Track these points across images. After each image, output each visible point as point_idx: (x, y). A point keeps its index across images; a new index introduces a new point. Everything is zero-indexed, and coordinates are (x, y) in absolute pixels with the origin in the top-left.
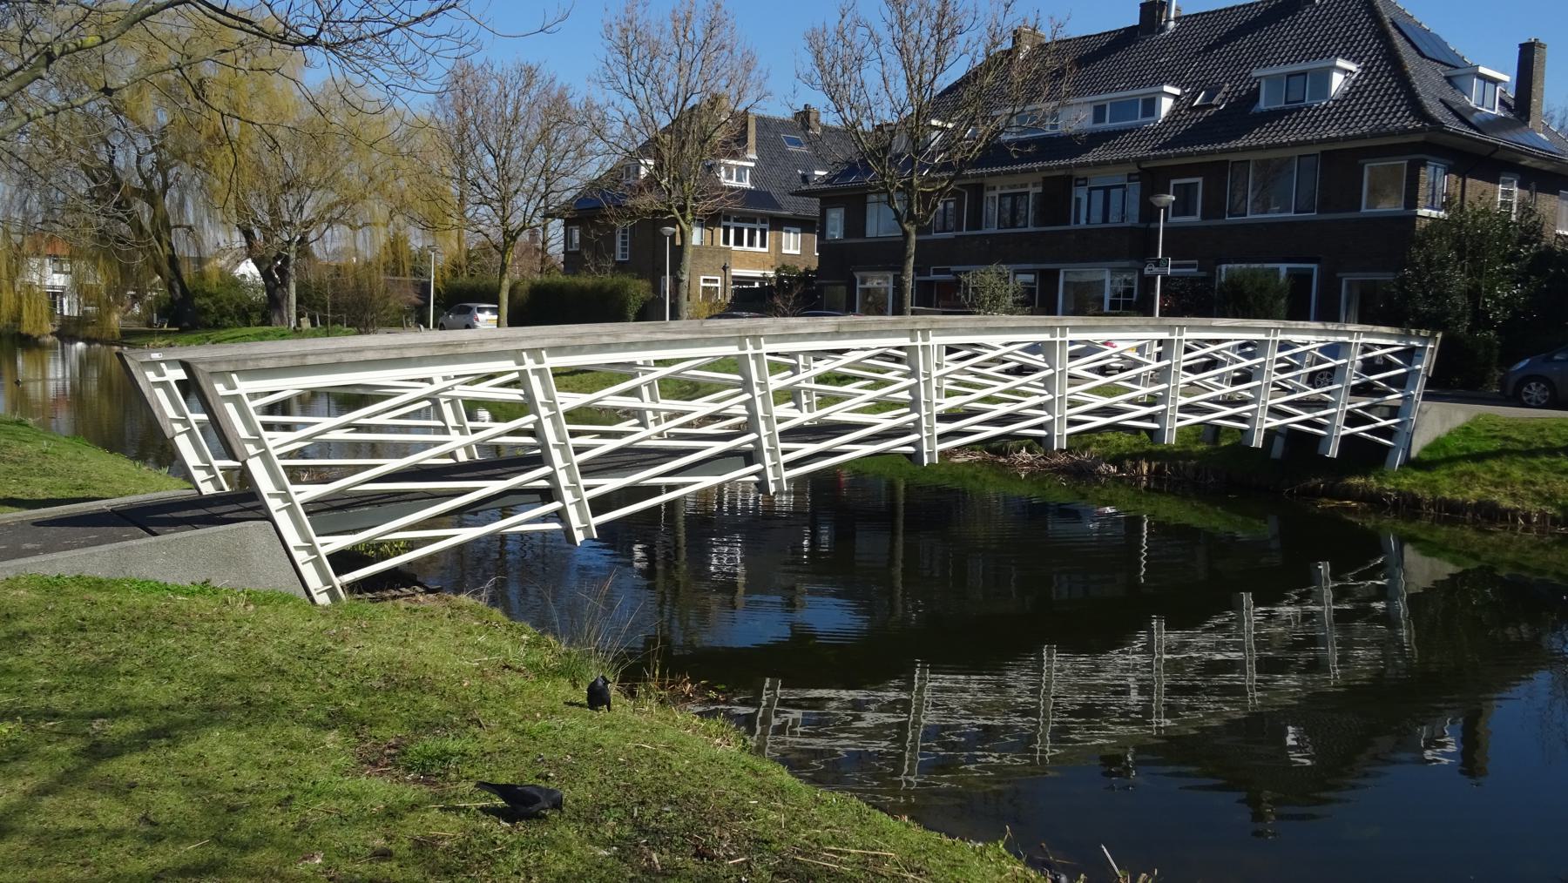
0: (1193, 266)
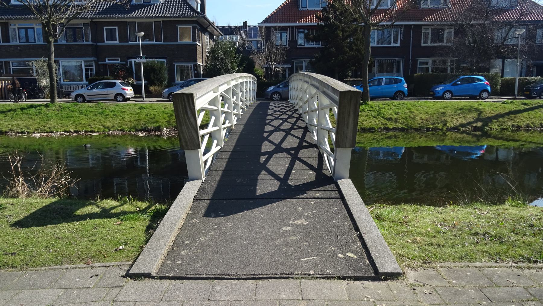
0: (118, 60)
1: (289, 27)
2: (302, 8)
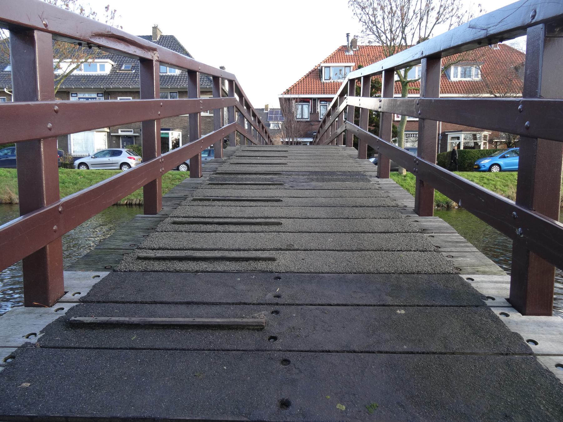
0: (131, 131)
1: (311, 99)
2: (325, 80)
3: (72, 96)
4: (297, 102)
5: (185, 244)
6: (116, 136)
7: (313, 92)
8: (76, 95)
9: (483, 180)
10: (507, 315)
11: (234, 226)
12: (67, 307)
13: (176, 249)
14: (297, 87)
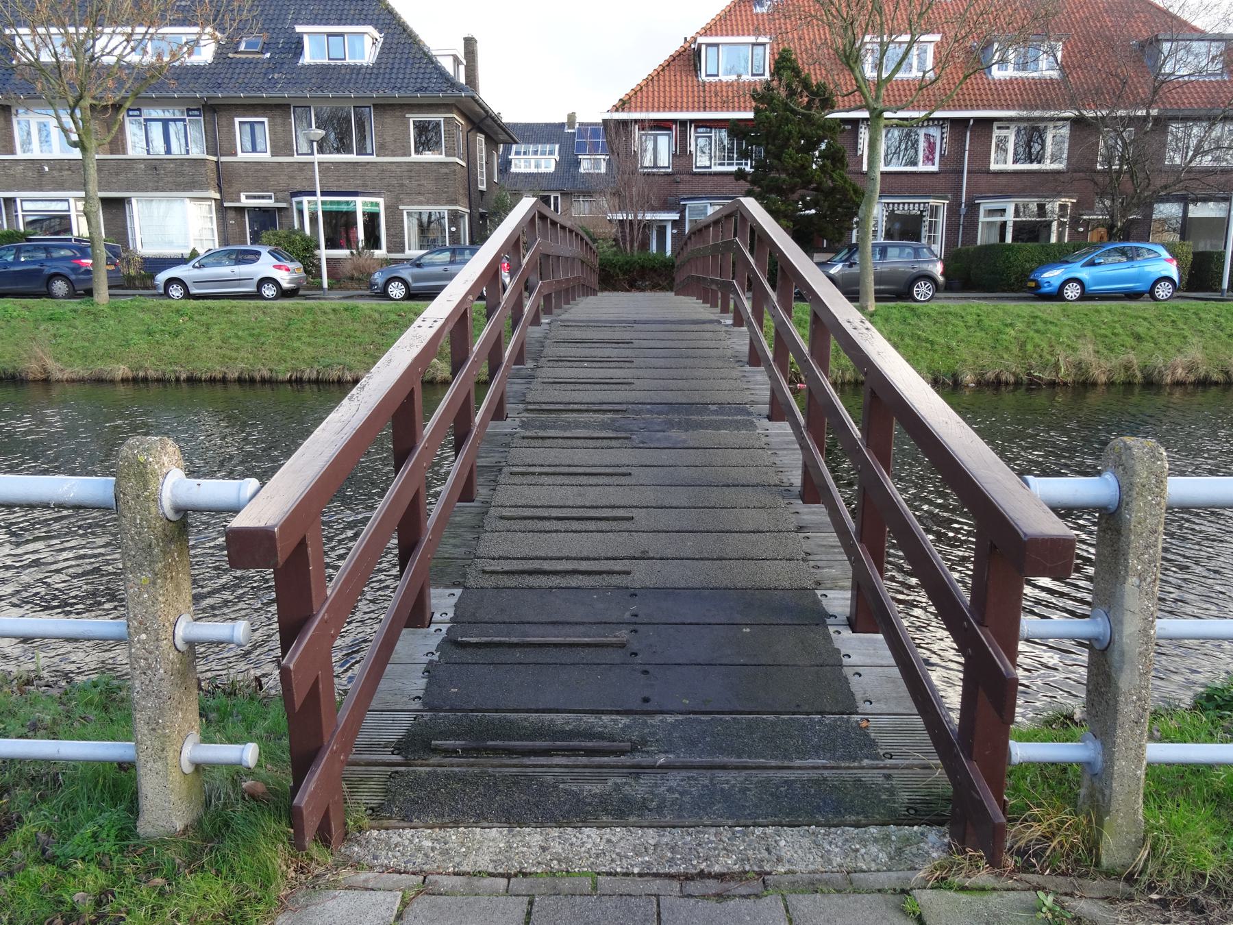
0: (270, 197)
2: (707, 75)
3: (129, 116)
4: (643, 129)
5: (526, 551)
6: (236, 209)
7: (679, 105)
8: (137, 113)
9: (1034, 323)
10: (839, 633)
11: (577, 523)
12: (444, 628)
13: (518, 559)
14: (645, 94)
